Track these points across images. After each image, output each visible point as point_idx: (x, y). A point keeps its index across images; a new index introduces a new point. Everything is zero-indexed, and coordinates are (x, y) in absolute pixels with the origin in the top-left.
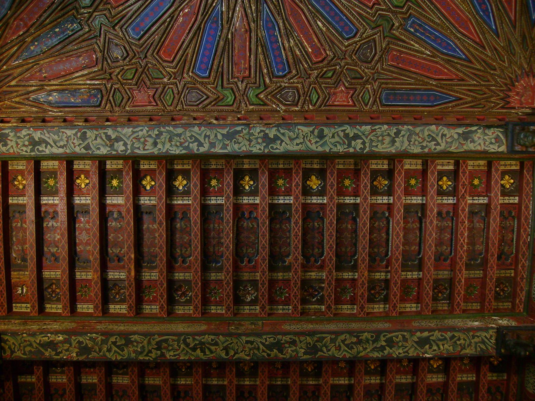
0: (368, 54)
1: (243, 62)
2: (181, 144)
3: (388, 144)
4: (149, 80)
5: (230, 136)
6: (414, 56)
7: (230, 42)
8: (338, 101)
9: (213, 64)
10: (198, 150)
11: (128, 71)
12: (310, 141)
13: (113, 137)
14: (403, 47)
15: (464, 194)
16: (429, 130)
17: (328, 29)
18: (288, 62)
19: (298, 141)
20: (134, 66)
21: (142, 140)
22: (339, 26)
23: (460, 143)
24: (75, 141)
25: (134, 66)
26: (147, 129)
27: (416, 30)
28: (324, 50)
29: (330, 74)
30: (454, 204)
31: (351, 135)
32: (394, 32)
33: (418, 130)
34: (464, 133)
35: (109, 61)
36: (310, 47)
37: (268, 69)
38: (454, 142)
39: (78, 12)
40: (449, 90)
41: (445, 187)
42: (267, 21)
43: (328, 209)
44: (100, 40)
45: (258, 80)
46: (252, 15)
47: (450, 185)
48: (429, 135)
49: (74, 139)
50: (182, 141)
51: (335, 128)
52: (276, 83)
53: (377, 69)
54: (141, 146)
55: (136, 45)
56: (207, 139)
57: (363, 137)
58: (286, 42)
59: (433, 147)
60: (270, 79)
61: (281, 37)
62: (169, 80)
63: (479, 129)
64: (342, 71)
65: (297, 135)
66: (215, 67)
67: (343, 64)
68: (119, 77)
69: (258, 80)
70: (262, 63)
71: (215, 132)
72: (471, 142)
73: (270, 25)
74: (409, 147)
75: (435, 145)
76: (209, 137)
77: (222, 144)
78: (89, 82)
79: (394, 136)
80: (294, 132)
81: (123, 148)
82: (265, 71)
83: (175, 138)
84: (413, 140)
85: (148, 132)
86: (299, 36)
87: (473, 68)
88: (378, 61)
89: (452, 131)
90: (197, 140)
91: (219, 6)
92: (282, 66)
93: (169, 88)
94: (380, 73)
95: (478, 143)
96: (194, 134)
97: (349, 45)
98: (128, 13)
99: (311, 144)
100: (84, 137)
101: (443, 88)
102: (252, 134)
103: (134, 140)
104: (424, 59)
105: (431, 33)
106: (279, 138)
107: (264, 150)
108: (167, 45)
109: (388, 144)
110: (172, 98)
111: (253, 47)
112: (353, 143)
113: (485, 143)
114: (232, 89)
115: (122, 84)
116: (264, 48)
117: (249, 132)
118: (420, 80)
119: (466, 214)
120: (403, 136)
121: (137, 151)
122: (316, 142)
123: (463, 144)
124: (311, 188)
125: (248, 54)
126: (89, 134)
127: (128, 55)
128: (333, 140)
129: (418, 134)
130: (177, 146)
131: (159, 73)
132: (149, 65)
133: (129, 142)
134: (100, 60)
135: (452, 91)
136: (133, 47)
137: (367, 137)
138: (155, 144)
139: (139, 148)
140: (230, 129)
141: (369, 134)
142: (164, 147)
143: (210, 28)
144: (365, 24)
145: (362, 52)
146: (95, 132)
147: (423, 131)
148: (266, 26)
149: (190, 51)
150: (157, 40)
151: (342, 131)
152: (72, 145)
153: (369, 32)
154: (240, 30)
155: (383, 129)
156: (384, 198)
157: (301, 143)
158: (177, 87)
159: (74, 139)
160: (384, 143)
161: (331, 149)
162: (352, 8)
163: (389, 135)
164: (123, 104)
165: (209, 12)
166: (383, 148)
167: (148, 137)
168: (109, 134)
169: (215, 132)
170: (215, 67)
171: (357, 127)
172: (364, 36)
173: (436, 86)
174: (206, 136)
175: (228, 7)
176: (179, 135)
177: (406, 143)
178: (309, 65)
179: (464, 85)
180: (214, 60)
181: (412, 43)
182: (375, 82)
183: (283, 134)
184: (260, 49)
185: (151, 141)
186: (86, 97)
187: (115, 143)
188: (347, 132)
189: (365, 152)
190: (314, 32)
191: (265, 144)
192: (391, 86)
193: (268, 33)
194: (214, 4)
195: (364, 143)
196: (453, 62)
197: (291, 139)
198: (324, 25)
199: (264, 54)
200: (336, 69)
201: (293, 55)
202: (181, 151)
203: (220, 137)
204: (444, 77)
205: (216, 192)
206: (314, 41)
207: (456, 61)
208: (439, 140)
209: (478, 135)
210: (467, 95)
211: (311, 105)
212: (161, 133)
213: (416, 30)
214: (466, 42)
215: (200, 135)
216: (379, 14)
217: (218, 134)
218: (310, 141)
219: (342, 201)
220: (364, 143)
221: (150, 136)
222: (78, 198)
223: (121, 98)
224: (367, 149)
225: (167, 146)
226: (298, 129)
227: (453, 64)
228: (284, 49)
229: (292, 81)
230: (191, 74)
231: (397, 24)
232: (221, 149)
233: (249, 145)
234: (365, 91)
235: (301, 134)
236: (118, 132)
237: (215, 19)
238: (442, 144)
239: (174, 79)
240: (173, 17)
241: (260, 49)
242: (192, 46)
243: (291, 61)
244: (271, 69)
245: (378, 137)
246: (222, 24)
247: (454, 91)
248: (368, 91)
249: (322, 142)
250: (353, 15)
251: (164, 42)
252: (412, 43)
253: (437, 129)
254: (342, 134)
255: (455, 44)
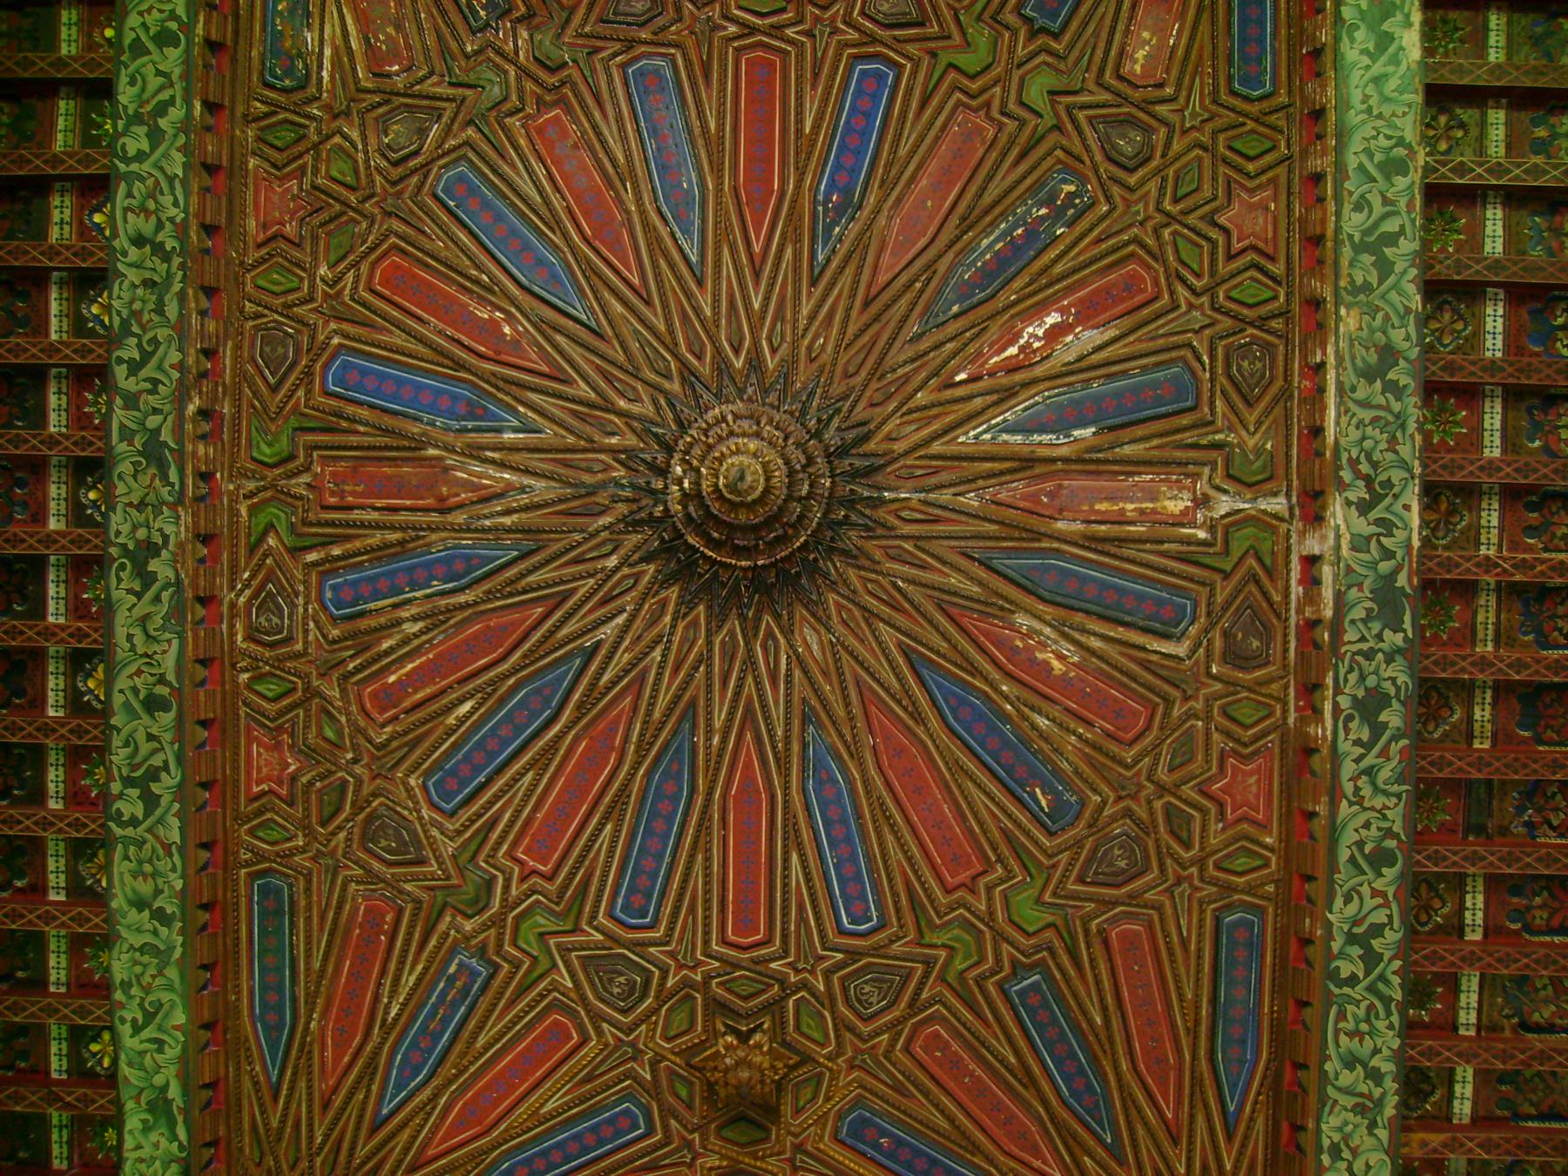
0: (384, 843)
1: (360, 489)
2: (137, 315)
3: (134, 890)
4: (322, 225)
5: (153, 453)
6: (383, 973)
7: (417, 454)
8: (259, 754)
9: (360, 403)
10: (120, 361)
11: (350, 162)
12: (139, 673)
13: (163, 123)
14: (407, 942)
15: (62, 1099)
16: (173, 1006)
17: (451, 731)
18: (362, 614)
19: (139, 639)
20: (364, 181)
21: (151, 205)
22: (458, 763)
23: (142, 1090)
24: (156, 14)
25: (364, 181)
26: (178, 220)
27: (452, 980)
28: (395, 718)
29: (329, 734)
30: (48, 1073)
31: (155, 788)
32: (448, 919)
33: (172, 973)
34: (168, 1102)
35: (381, 110)
36: (399, 681)
37: (338, 558)
38: (142, 1074)
39: (519, 20)
40: (296, 1067)
41: (95, 1047)
42: (468, 558)
43: (17, 720)
44: (438, 84)
45: (313, 530)
46: (486, 517)
47: (100, 1062)
48: (161, 1005)
49: (161, 11)
50: (146, 317)
51: (172, 743)
52: (305, 582)
53: (346, 866)
54: (135, 203)
55: (420, 187)
56: (148, 386)
57: (152, 819)
58: (414, 610)
59: (128, 1016)
60: (315, 564)
61: (428, 596)
62: (322, 280)
63: (181, 1147)
64: (341, 769)
65: (154, 638)
66: (350, 409)
67: (358, 769)
68: (337, 139)
69: (313, 530)
70: (358, 544)
71: (167, 408)
72: (144, 1121)
73: (459, 567)
74: (125, 947)
75: (134, 1020)
76: (153, 392)
77: (134, 426)
78: (328, 52)
79: (156, 905)
80: (163, 628)
81: (131, 152)
82: (336, 551)
83: (154, 298)
84: (146, 959)
85: (171, 220)
86: (434, 647)
87: (743, 287)
88: (369, 871)
89: (173, 1070)
90: (146, 357)
91: (516, 423)
92: (349, 599)
93: (301, 279)
94: (335, 876)
95: (144, 1143)
96: (162, 349)
97: (409, 790)
98: (513, 166)
99: (130, 677)
100: (165, 39)
101: (301, 1050)
102: (157, 513)
103: (150, 182)
104: (376, 998)
105: (445, 1022)
106: (147, 586)
107: (115, 545)
108: (415, 276)
109: (134, 890)
110: (275, 289)
111: (402, 517)
112: (134, 792)
113: (142, 1160)
114: (292, 457)
115: (316, 146)
116: (398, 549)
117: (164, 503)
118: (318, 984)
119: (39, 1107)
120: (155, 933)
121: (122, 189)
122: (135, 690)
123: (138, 1102)
124: (89, 675)
125: (379, 503)
126: (174, 54)
127: (395, 164)
128: (141, 736)
129: (161, 973)
130: (131, 302)
131: (342, 252)
132: (364, 225)
133: (146, 167)
134: (386, 84)
135: (295, 1074)
136: (415, 179)
137: (149, 830)
138: (139, 241)
139: (130, 195)
140: (171, 450)
141: (157, 837)
142: (130, 265)
143: (455, 397)
144: (467, 835)
145: (388, 826)
146: (177, 72)
147: (170, 988)
148: (455, 557)
149: (398, 339)
150: (428, 246)
151: (166, 762)
152: (145, 7)
153: (449, 848)
154: (446, 483)
155: (172, 876)
156: (63, 877)
157: (133, 648)
158: (302, 303)
159: (161, 11)
160: (135, 878)
161: (119, 731)
162: (510, 801)
163: (158, 892)
164: (266, 149)
165: (500, 395)
166: (121, 874)
167: (159, 220)
168: (172, 110)
169: (167, 408)
170: (350, 409)
171: (177, 806)
172: (435, 832)
173: (307, 1029)
174: (155, 382)
175: (514, 448)
176: (160, 310)
177: (138, 940)
178: (352, 674)
179: (310, 1111)
180: (372, 406)
181: (420, 968)
182: (312, 858)
183: (157, 599)
184: (394, 536)
185: (147, 228)
186: (288, 44)
187: (145, 129)
188: (163, 775)
189: (112, 825)
190: (442, 692)
191: (131, 547)
192: (303, 903)
193: (438, 560)
194: (521, 409)
195: (134, 822)
196: (372, 1080)
197: (143, 621)
198: (461, 721)
199: (380, 548)
200: (345, 750)
201: (376, 630)
202: (119, 314)
203: (153, 421)
204: (329, 1054)
205: (79, 408)
206: (415, 692)
207: (374, 1088)
208: (147, 1033)
209: (164, 1142)
210: (285, 1115)
211: (250, 679)
212: (166, 258)
213: (452, 980)
214: (426, 1120)
215: (160, 368)
216: (495, 877)
217: (159, 418)
218: (139, 673)
219: (52, 760)
220: (134, 822)
221: (160, 226)
222: (74, 18)
223: (278, 143)
224: (118, 831)
225: (133, 276)
226: (169, 641)
227: (366, 1081)
228: (395, 606)
229: (312, 625)
230: (336, 341)
231: (468, 926)
232: (122, 426)
233: (130, 504)
234: (287, 830)
235: (156, 648)
236: (175, 136)
237: (479, 412)
238: (136, 1039)
239: (325, 294)
240: (493, 292)
241: (394, 536)
242: (412, 346)
243: (364, 624)
244: (343, 568)
245: (150, 861)
246: (465, 430)
247: (293, 1083)
248: (289, 840)
249: (137, 705)
250: (491, 803)
251: (427, 265)
252: (420, 968)
253: (177, 1028)
254: (157, 761)
255: (419, 1088)
